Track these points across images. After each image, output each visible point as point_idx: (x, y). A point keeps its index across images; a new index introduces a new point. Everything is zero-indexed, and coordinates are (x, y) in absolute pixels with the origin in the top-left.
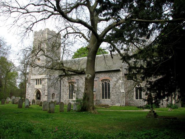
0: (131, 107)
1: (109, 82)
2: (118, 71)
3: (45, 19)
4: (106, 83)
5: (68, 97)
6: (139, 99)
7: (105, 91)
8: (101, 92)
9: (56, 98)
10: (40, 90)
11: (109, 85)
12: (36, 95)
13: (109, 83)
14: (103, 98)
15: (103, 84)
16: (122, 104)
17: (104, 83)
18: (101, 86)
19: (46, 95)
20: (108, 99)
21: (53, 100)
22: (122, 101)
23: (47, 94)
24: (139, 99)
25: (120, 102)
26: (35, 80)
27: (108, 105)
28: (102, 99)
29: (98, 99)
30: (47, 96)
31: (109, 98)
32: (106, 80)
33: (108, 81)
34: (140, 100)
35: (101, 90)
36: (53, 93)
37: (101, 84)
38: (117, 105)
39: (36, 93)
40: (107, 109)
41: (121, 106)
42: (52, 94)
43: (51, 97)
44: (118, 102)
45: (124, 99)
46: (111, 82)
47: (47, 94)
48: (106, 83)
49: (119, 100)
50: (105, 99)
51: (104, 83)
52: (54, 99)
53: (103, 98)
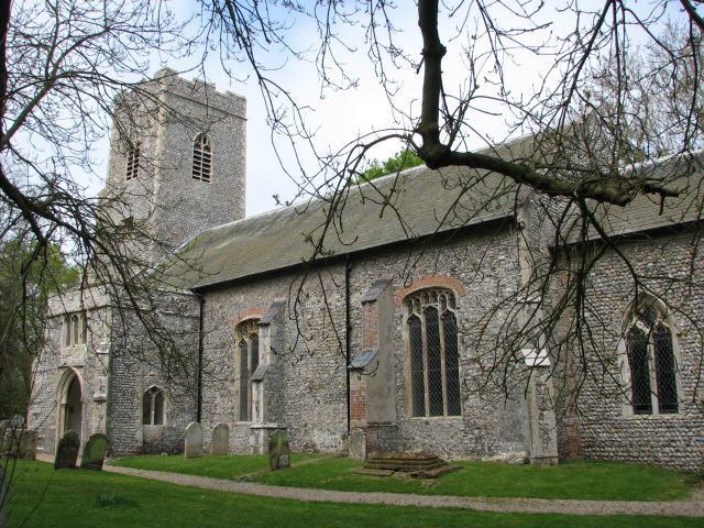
0: (602, 471)
1: (453, 305)
2: (506, 226)
3: (362, 154)
4: (430, 311)
5: (237, 411)
6: (427, 415)
7: (430, 367)
8: (407, 374)
9: (172, 416)
10: (79, 372)
11: (451, 329)
12: (64, 401)
13: (448, 315)
14: (420, 411)
15: (413, 320)
16: (537, 451)
17: (422, 317)
18: (406, 335)
19: (100, 401)
20: (447, 419)
21: (152, 426)
22: (536, 427)
23: (105, 395)
24: (427, 415)
25: (525, 432)
26: (62, 319)
27: (433, 461)
28: (241, 419)
29: (392, 417)
30: (105, 405)
31: (455, 410)
32: (435, 296)
33: (444, 302)
34: (667, 416)
35: (407, 362)
36: (154, 389)
37: (405, 320)
38: (503, 456)
39: (66, 388)
40: (419, 491)
41: (527, 461)
42: (147, 396)
43: (139, 413)
44: (513, 433)
45: (550, 416)
46: (460, 302)
47: (105, 395)
48: (430, 311)
49: (516, 423)
50: (432, 414)
51: (422, 317)
52: (158, 420)
53: (420, 411)
